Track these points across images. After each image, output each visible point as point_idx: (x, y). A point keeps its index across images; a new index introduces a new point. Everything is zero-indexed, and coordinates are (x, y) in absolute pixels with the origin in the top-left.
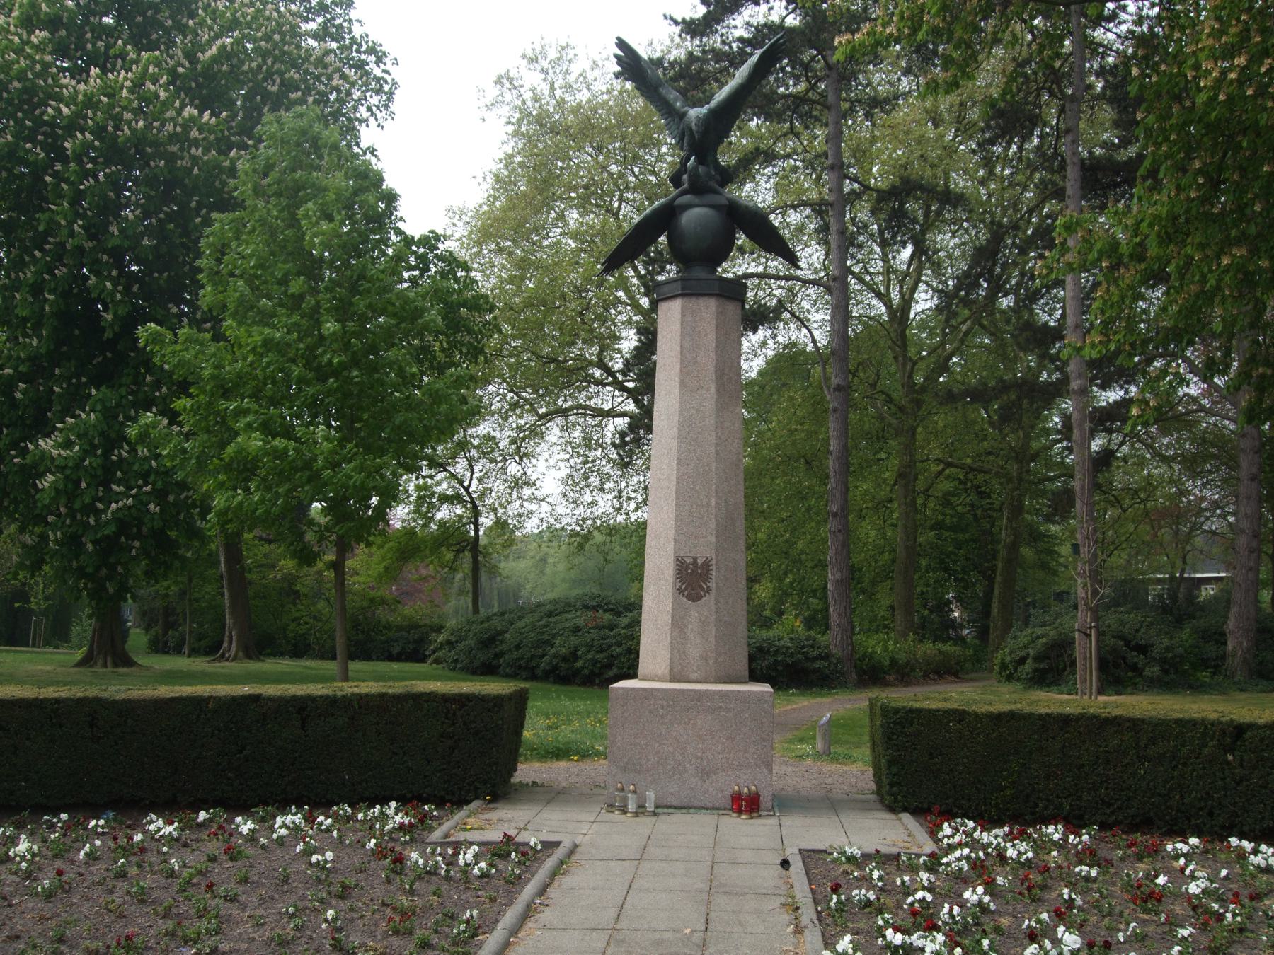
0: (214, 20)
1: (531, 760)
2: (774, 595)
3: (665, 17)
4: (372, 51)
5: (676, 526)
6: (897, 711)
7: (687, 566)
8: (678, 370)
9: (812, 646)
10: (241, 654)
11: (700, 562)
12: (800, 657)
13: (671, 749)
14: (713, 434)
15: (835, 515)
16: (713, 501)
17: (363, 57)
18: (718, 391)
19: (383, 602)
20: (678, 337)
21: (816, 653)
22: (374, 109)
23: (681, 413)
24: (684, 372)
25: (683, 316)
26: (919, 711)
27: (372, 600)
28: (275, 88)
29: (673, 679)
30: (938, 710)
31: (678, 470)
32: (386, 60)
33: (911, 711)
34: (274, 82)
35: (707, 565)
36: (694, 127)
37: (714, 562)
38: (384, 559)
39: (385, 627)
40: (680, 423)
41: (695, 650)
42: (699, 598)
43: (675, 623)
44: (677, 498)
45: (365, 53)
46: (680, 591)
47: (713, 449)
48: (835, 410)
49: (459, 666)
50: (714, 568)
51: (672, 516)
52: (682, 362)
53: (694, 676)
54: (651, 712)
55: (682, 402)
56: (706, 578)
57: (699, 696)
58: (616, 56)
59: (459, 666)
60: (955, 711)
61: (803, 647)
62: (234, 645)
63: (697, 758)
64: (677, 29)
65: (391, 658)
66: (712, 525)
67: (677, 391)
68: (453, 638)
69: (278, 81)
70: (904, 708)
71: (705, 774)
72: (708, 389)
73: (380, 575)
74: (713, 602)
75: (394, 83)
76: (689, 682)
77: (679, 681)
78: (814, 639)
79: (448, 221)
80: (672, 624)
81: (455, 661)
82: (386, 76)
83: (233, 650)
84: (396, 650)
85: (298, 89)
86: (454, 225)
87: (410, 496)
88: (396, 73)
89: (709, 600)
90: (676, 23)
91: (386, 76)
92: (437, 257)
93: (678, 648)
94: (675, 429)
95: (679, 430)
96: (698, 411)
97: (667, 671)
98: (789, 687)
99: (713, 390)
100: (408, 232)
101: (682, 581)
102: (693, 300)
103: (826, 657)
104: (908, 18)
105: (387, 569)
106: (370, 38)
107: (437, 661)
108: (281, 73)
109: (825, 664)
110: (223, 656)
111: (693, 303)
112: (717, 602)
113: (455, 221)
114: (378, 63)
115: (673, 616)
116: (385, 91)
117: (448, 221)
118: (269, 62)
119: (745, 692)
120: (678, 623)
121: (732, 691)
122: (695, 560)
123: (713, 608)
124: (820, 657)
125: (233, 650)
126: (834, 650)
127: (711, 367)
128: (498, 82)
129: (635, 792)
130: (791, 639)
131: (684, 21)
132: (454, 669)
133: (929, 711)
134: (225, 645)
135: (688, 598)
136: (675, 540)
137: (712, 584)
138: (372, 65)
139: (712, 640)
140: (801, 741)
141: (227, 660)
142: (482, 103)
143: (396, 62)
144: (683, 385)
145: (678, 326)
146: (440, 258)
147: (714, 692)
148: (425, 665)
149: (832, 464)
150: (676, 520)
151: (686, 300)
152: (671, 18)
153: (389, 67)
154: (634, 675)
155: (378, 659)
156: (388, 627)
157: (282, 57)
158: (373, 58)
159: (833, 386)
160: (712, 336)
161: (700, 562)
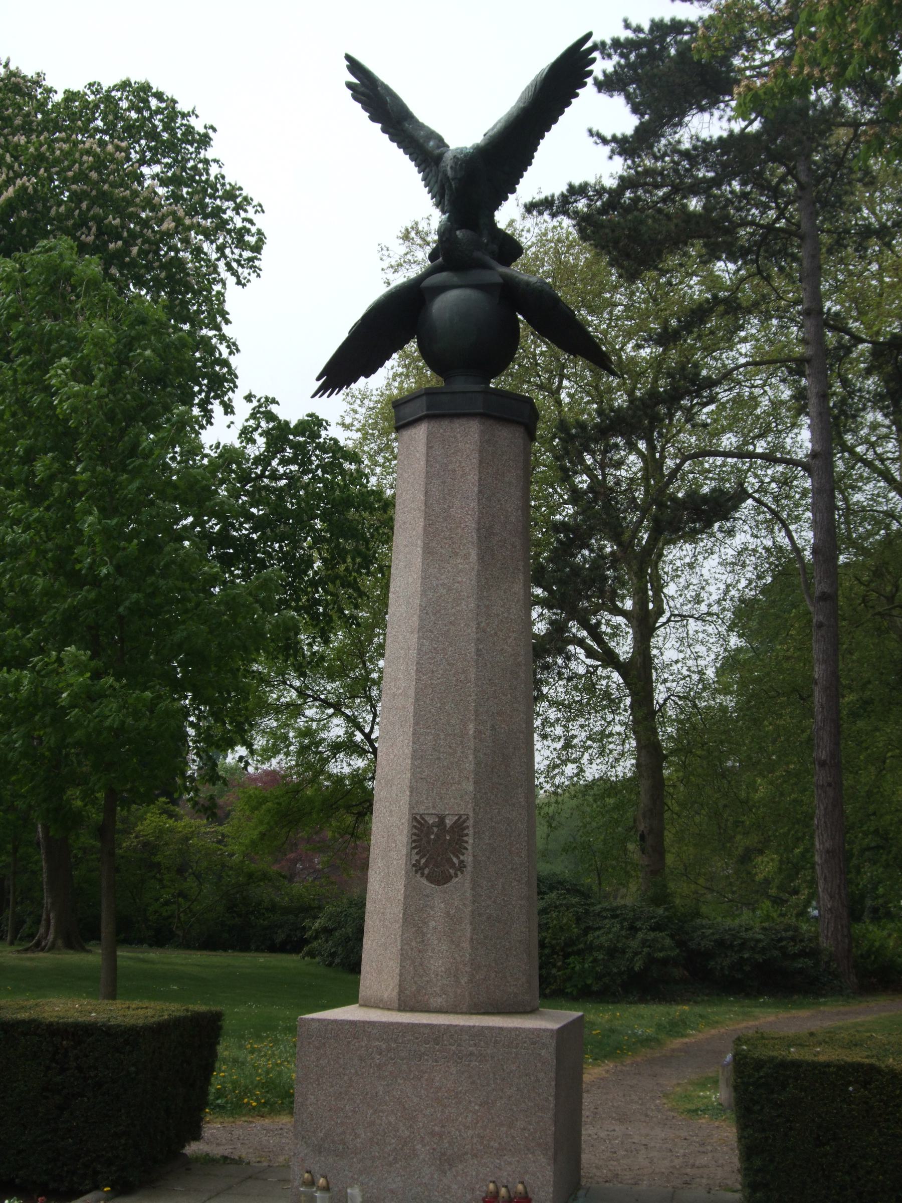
0: (16, 158)
1: (279, 1113)
2: (780, 869)
3: (591, 133)
4: (230, 195)
5: (414, 769)
6: (759, 1064)
7: (430, 827)
8: (420, 530)
9: (793, 939)
10: (60, 942)
11: (449, 822)
12: (776, 953)
13: (392, 1119)
14: (473, 624)
15: (823, 764)
16: (471, 728)
17: (218, 202)
18: (481, 558)
19: (265, 877)
20: (422, 481)
21: (796, 949)
22: (234, 265)
23: (424, 593)
24: (431, 532)
25: (429, 447)
26: (796, 1065)
27: (250, 876)
28: (91, 238)
29: (404, 1006)
30: (828, 1065)
31: (418, 680)
32: (249, 208)
33: (784, 1065)
34: (89, 229)
35: (459, 827)
36: (450, 173)
37: (470, 823)
38: (261, 822)
39: (267, 909)
40: (423, 609)
41: (437, 963)
42: (447, 879)
43: (408, 919)
44: (416, 723)
45: (221, 198)
46: (417, 868)
47: (472, 648)
48: (820, 626)
49: (337, 960)
50: (470, 831)
51: (408, 751)
52: (427, 516)
53: (438, 1001)
54: (361, 1059)
55: (426, 577)
56: (458, 846)
57: (437, 1034)
58: (349, 85)
59: (337, 960)
60: (857, 1067)
61: (781, 940)
62: (52, 930)
63: (432, 1134)
64: (607, 150)
65: (273, 949)
66: (469, 765)
67: (418, 561)
68: (330, 925)
69: (94, 229)
70: (772, 1059)
71: (446, 1161)
72: (466, 557)
73: (253, 842)
74: (468, 885)
75: (259, 232)
76: (428, 1011)
77: (413, 1010)
78: (796, 929)
79: (347, 407)
80: (405, 919)
81: (333, 955)
82: (248, 225)
83: (51, 937)
84: (280, 937)
85: (120, 237)
86: (356, 412)
87: (291, 744)
88: (261, 223)
89: (462, 883)
90: (605, 141)
91: (248, 225)
92: (319, 446)
93: (412, 958)
94: (416, 618)
95: (421, 619)
96: (450, 590)
97: (395, 993)
98: (760, 993)
99: (473, 557)
100: (282, 417)
101: (421, 852)
102: (445, 423)
103: (814, 953)
104: (835, 51)
105: (263, 835)
106: (227, 181)
107: (311, 954)
108: (99, 220)
109: (810, 963)
110: (38, 944)
111: (445, 428)
112: (475, 885)
113: (356, 407)
114: (238, 209)
115: (406, 907)
116: (250, 244)
117: (347, 407)
118: (84, 206)
119: (510, 1030)
120: (413, 919)
121: (490, 1029)
122: (442, 819)
123: (469, 894)
124: (803, 954)
125: (51, 937)
126: (825, 943)
127: (471, 523)
128: (406, 237)
129: (327, 1189)
130: (764, 929)
131: (614, 139)
132: (330, 965)
133: (814, 1065)
134: (42, 930)
135: (430, 879)
136: (412, 789)
137: (468, 858)
138: (230, 213)
139: (466, 945)
140: (703, 1085)
141: (43, 950)
142: (385, 265)
143: (260, 209)
144: (428, 551)
145: (423, 463)
146: (322, 448)
147: (462, 1029)
148: (295, 957)
149: (818, 697)
150: (414, 757)
151: (435, 425)
152: (599, 135)
153: (251, 214)
154: (351, 997)
155: (258, 950)
156: (273, 908)
157: (103, 199)
158: (231, 204)
159: (817, 594)
160: (473, 477)
161: (449, 822)
